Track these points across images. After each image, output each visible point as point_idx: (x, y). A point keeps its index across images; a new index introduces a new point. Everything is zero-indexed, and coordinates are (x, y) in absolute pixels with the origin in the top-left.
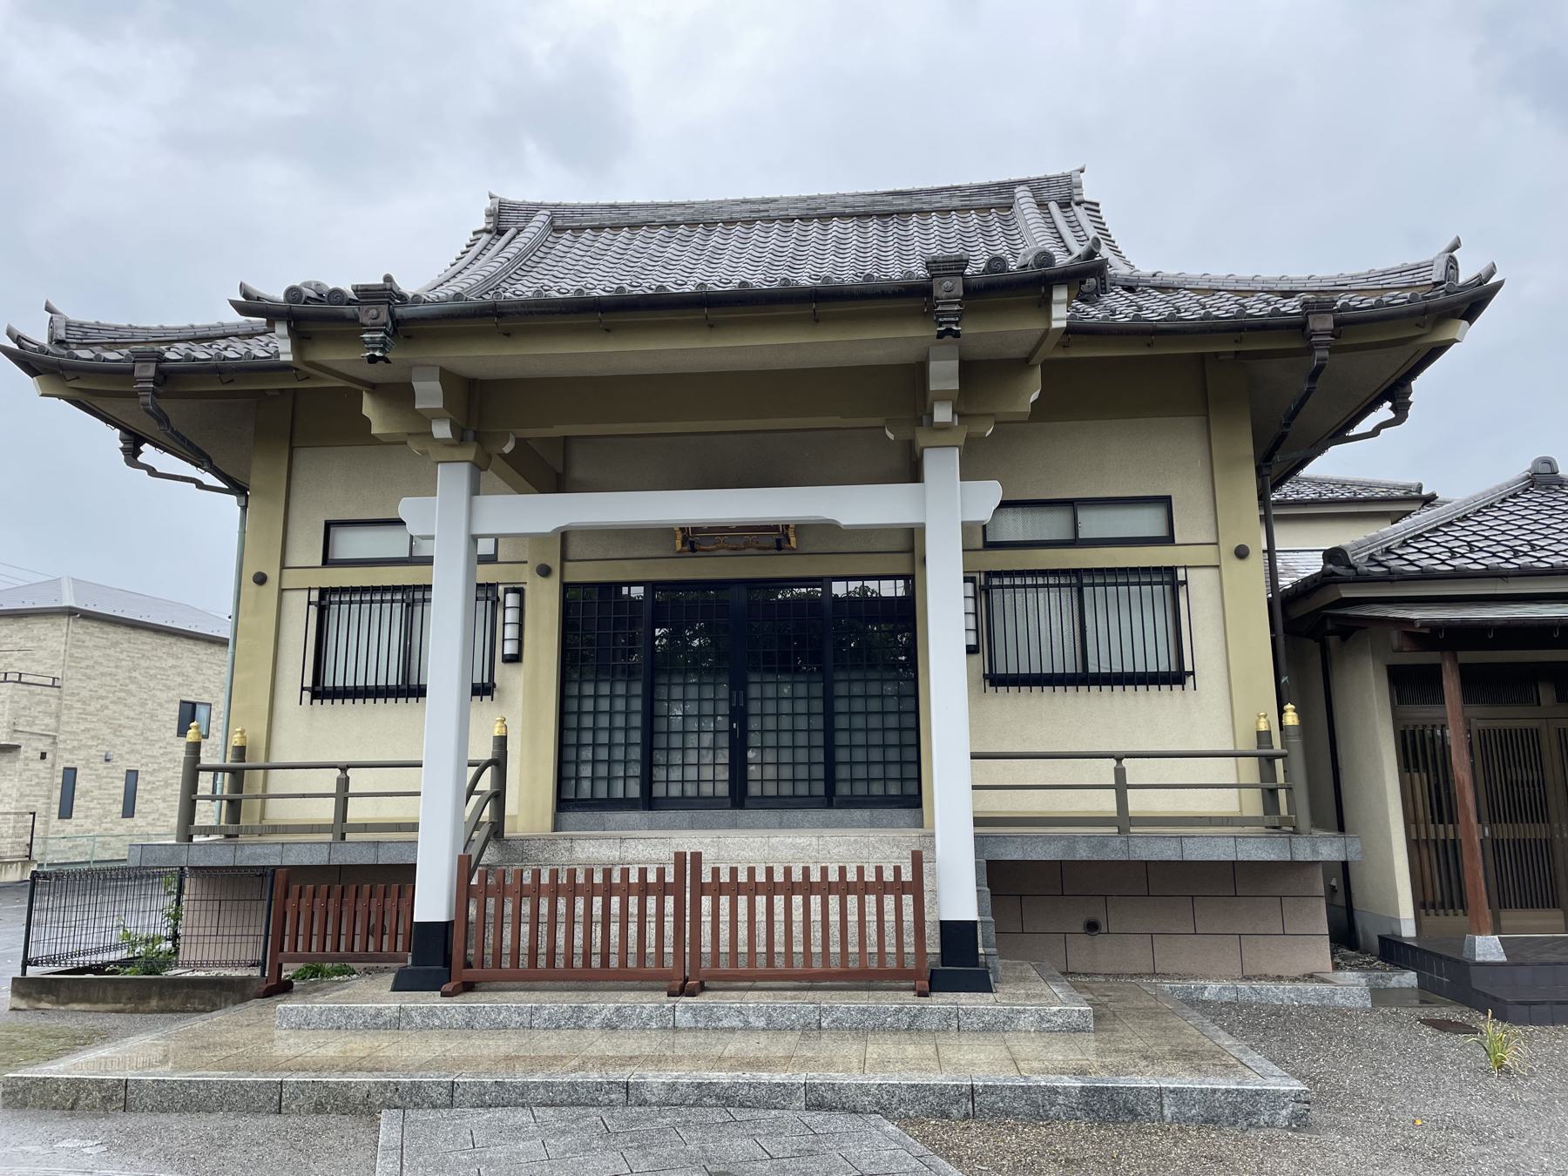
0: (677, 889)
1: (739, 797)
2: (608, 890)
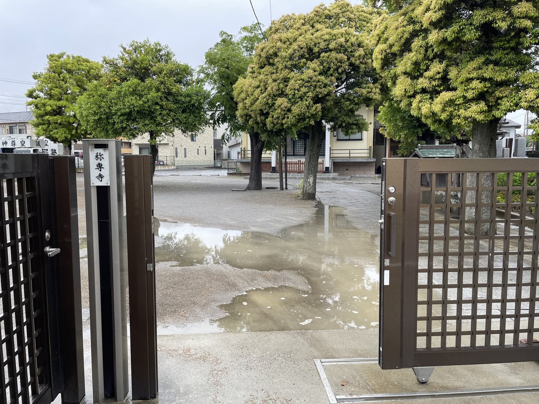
0: (298, 164)
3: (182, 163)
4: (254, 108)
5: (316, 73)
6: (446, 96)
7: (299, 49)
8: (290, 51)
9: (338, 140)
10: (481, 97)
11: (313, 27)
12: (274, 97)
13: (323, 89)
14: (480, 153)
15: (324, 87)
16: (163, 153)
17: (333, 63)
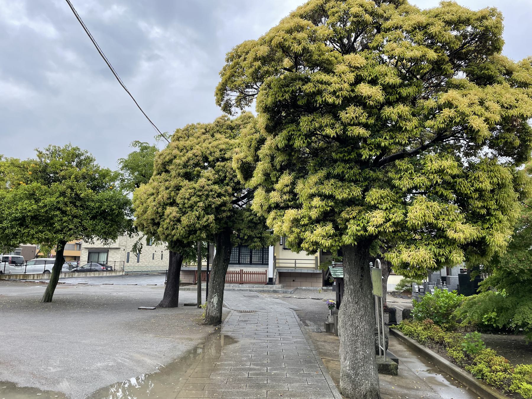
1: (251, 263)
2: (233, 273)
3: (134, 268)
4: (145, 216)
5: (210, 182)
6: (291, 213)
7: (194, 157)
8: (184, 159)
9: (285, 249)
10: (325, 217)
11: (213, 136)
12: (164, 206)
13: (217, 199)
14: (350, 285)
15: (217, 197)
16: (113, 258)
17: (229, 173)
